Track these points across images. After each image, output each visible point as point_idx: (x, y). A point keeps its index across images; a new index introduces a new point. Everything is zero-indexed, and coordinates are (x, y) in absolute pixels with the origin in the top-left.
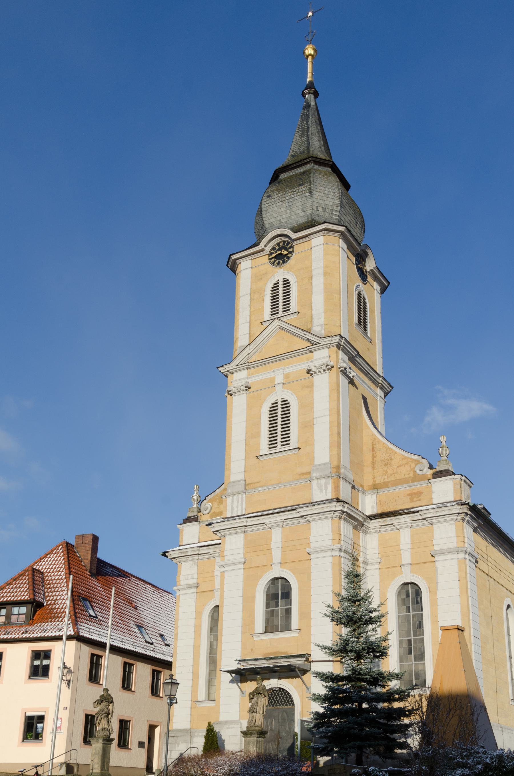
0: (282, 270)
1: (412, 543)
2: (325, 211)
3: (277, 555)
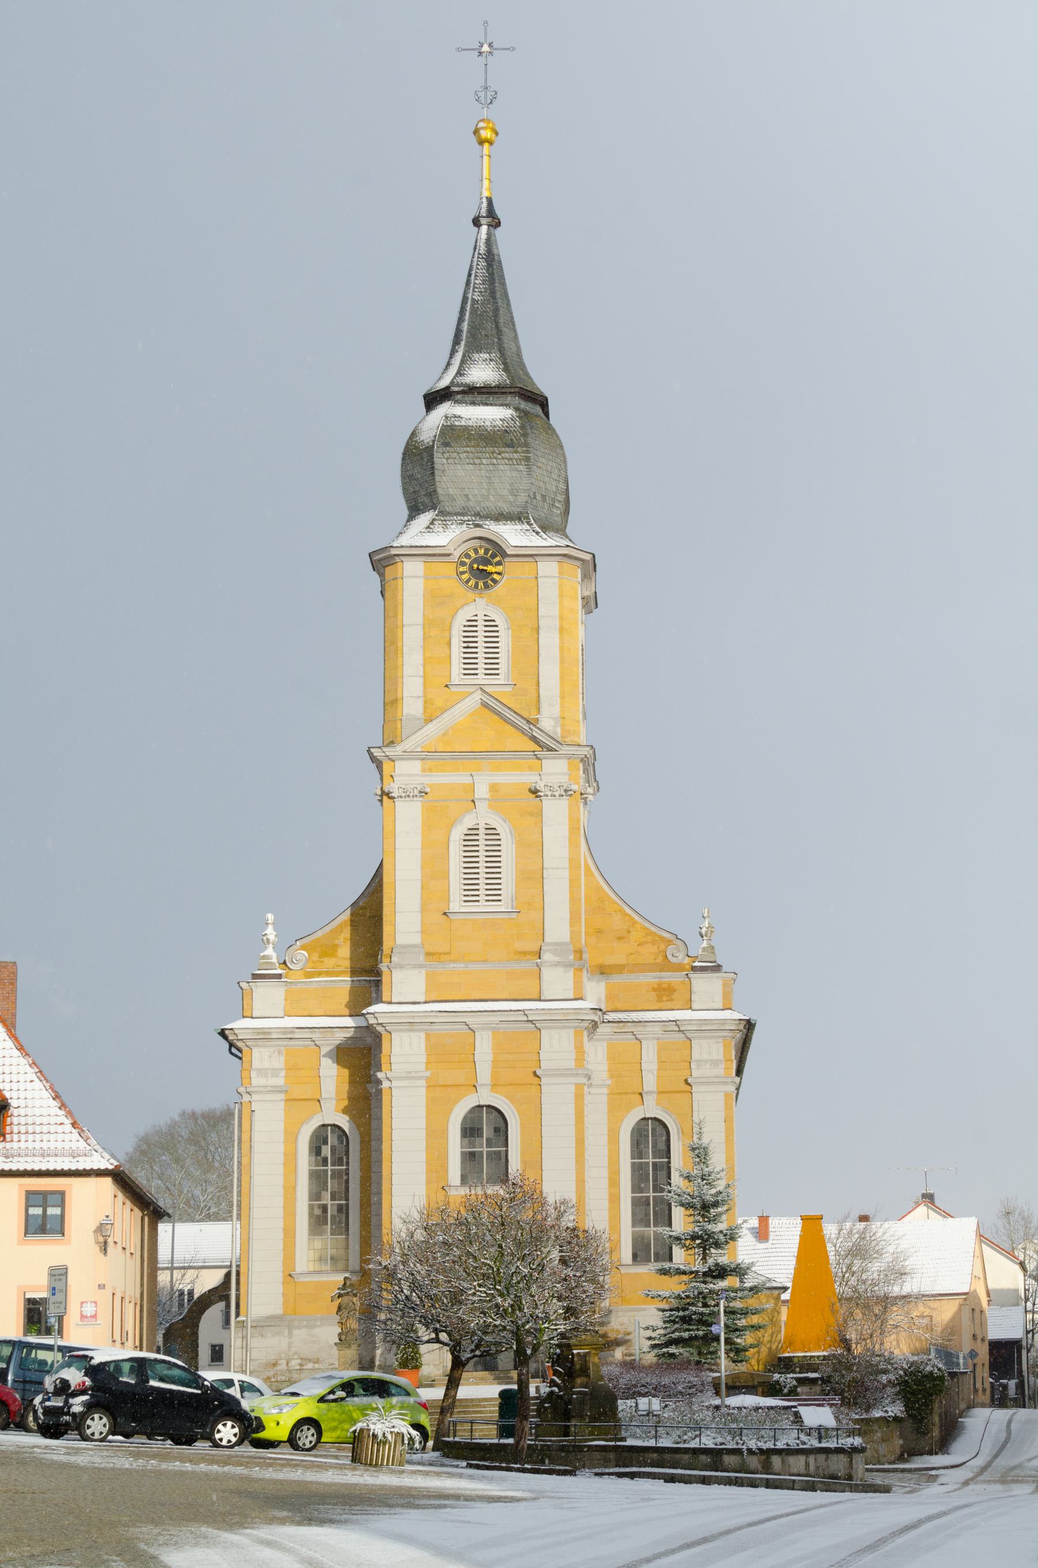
1: (661, 1062)
2: (544, 501)
3: (484, 1073)
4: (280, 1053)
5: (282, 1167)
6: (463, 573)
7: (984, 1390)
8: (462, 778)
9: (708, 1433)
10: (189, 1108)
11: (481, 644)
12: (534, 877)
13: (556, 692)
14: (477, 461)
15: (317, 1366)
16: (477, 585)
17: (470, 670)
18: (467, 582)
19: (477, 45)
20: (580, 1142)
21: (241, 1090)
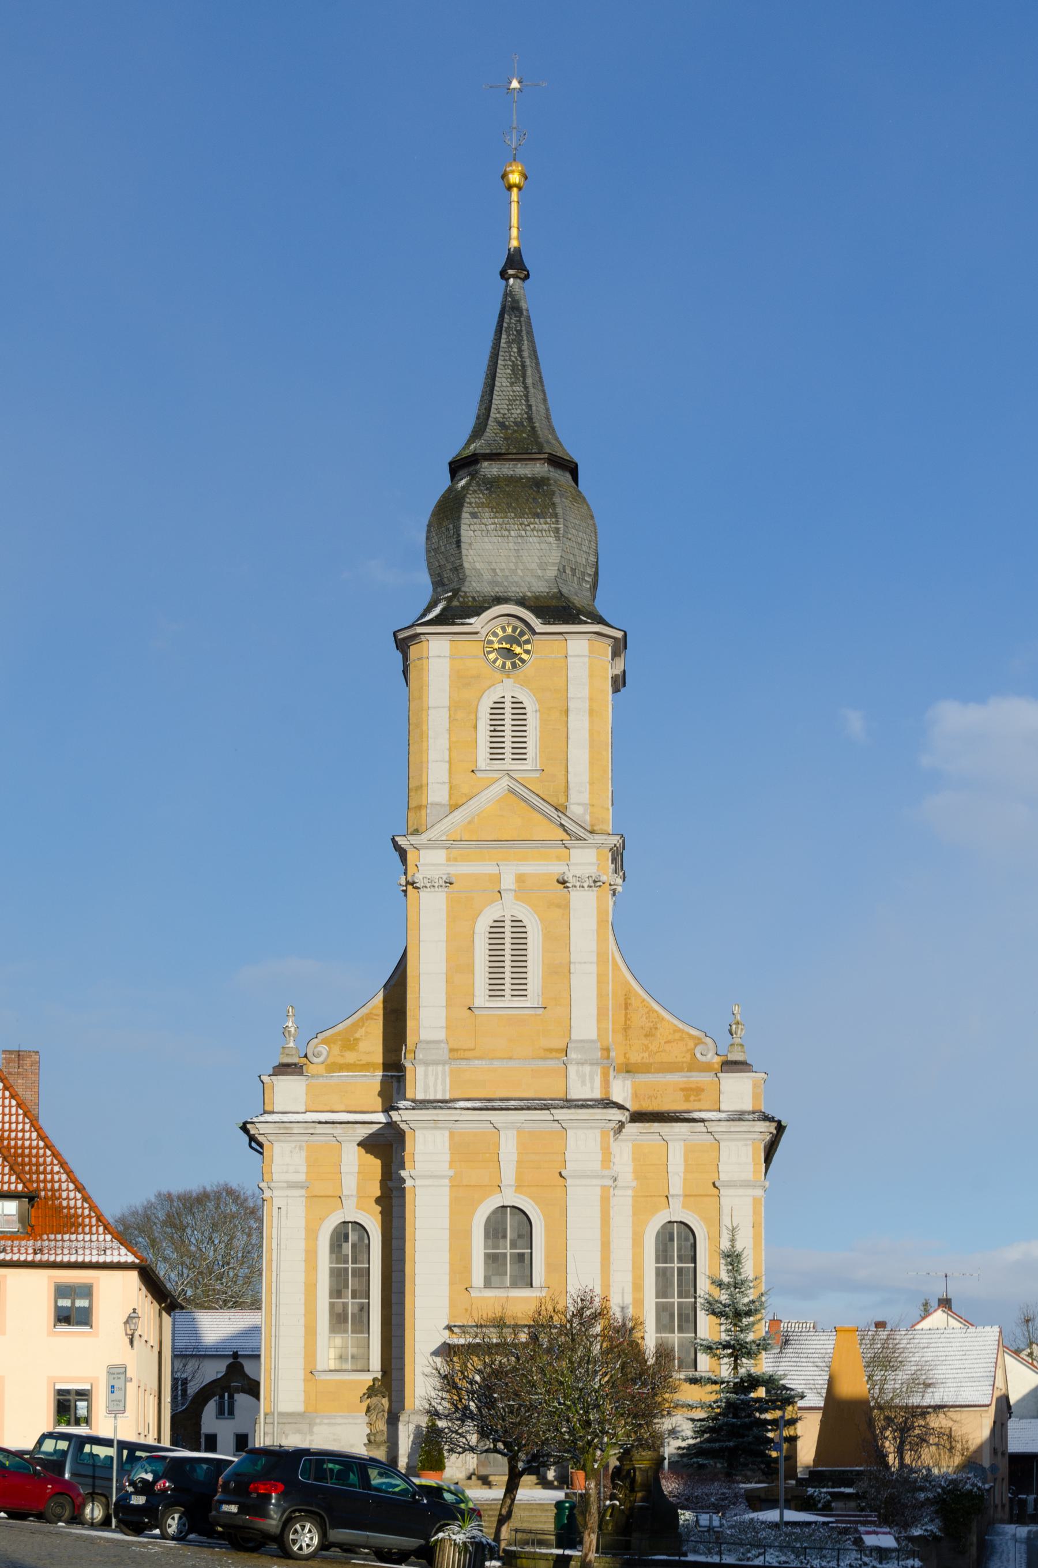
0: (511, 680)
2: (574, 575)
3: (509, 1173)
4: (300, 1148)
5: (303, 1263)
7: (1003, 1506)
8: (489, 868)
9: (772, 1551)
10: (164, 1190)
11: (508, 728)
12: (560, 972)
13: (586, 778)
16: (504, 665)
17: (496, 754)
18: (495, 661)
21: (263, 1185)
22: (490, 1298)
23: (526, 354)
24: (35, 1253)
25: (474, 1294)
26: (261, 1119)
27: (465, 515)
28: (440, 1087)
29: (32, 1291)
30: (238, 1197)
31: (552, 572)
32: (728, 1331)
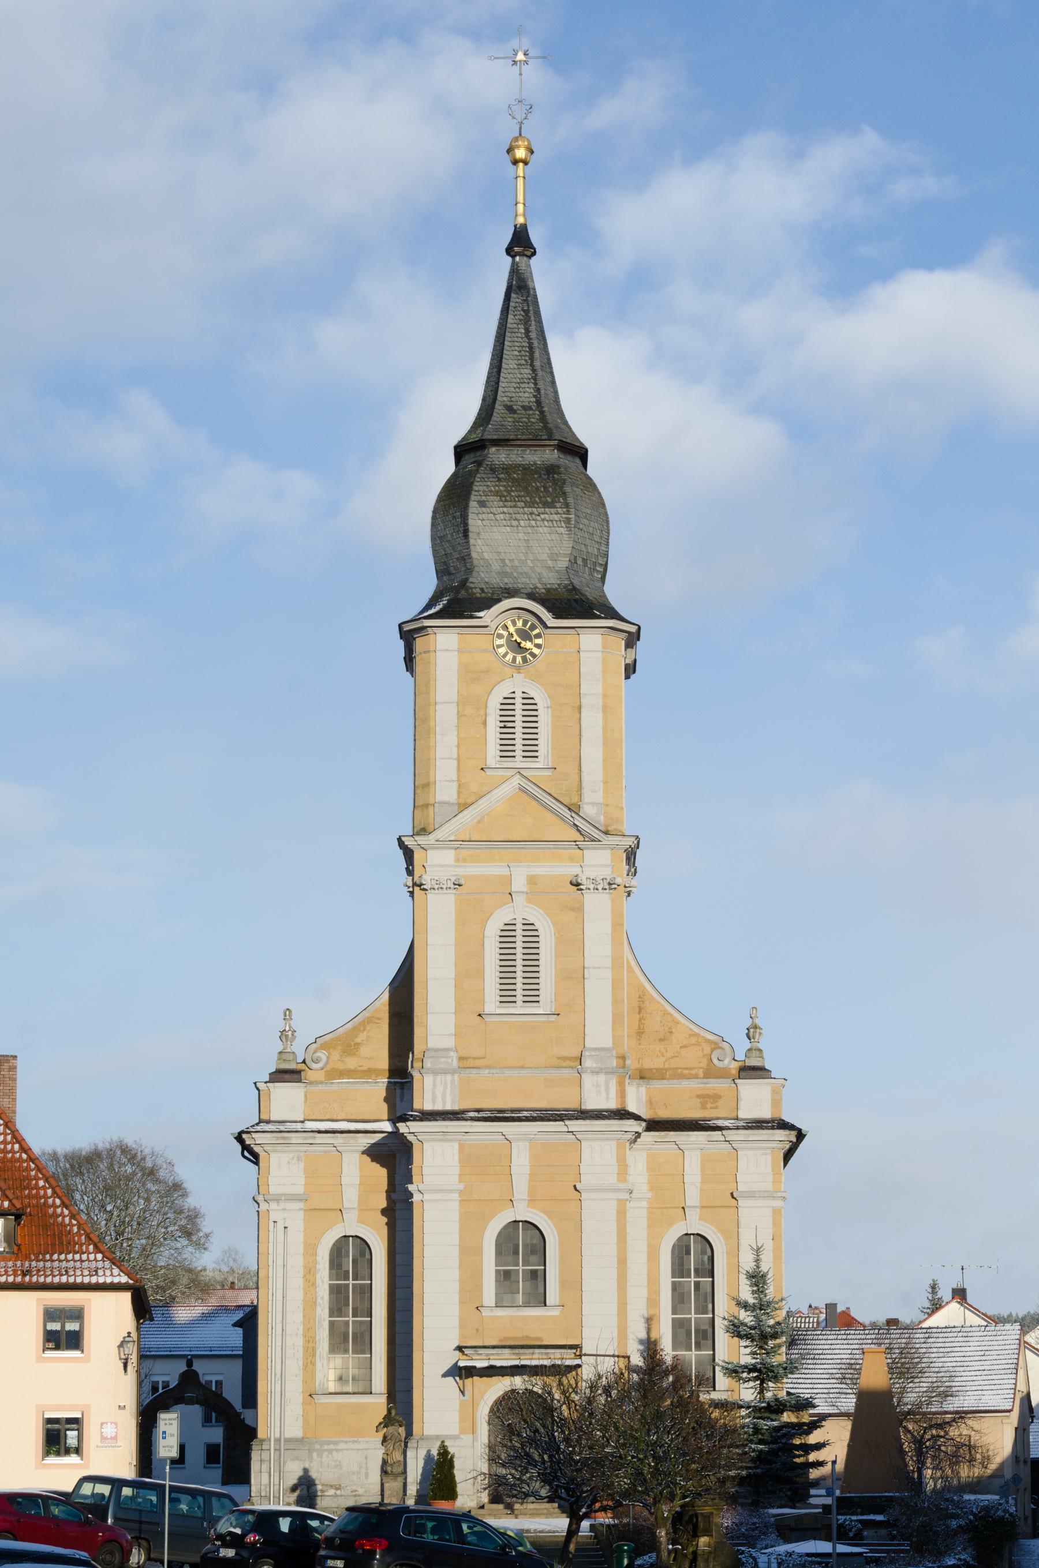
2: (585, 565)
4: (299, 1159)
6: (499, 646)
7: (1026, 1518)
11: (519, 724)
12: (574, 977)
13: (599, 777)
14: (515, 523)
15: (338, 1492)
17: (506, 751)
19: (511, 54)
20: (622, 1261)
22: (502, 1317)
23: (533, 335)
24: (24, 1275)
25: (485, 1313)
26: (258, 1128)
27: (473, 504)
28: (448, 1098)
29: (23, 1312)
30: (134, 1157)
31: (563, 563)
32: (754, 1353)
